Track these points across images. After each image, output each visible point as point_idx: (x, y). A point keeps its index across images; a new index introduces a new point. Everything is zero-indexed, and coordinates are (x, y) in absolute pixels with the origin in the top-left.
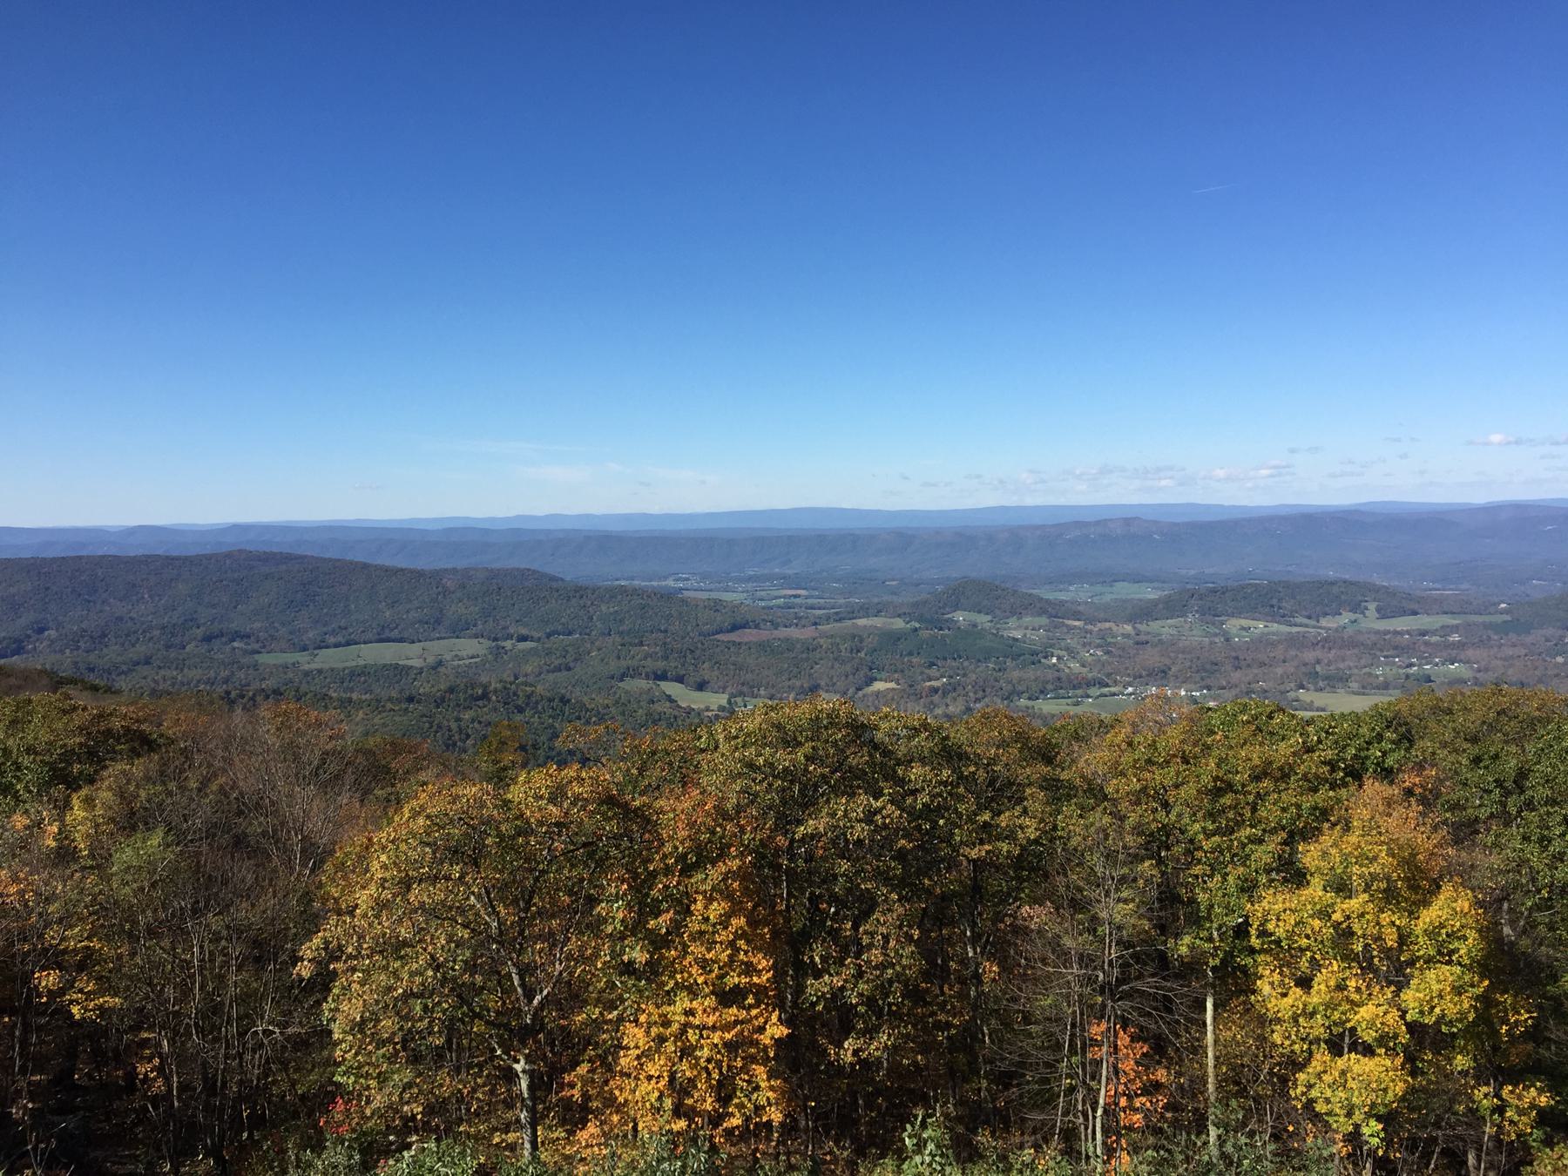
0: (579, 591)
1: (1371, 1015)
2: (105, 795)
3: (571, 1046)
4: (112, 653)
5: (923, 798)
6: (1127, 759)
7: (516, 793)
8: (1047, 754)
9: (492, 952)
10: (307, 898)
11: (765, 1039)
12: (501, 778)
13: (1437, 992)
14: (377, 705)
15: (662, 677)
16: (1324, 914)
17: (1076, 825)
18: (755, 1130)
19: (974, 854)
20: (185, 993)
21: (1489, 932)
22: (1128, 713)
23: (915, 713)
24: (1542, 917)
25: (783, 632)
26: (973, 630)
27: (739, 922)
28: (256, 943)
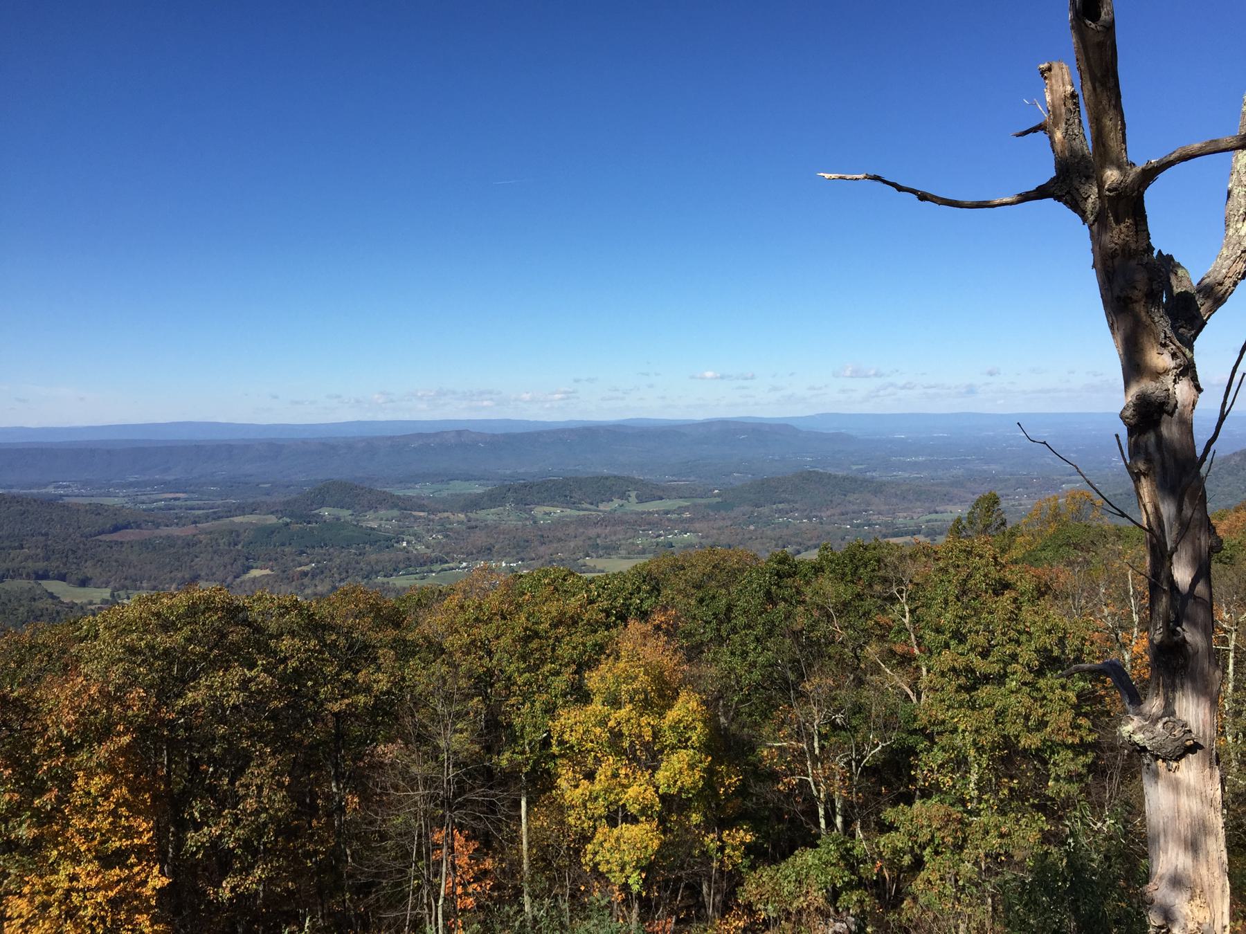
5: (293, 663)
6: (460, 618)
8: (395, 620)
11: (147, 891)
13: (679, 769)
15: (45, 576)
16: (603, 723)
19: (336, 707)
21: (710, 720)
22: (458, 585)
23: (286, 593)
24: (744, 708)
25: (164, 531)
27: (121, 792)
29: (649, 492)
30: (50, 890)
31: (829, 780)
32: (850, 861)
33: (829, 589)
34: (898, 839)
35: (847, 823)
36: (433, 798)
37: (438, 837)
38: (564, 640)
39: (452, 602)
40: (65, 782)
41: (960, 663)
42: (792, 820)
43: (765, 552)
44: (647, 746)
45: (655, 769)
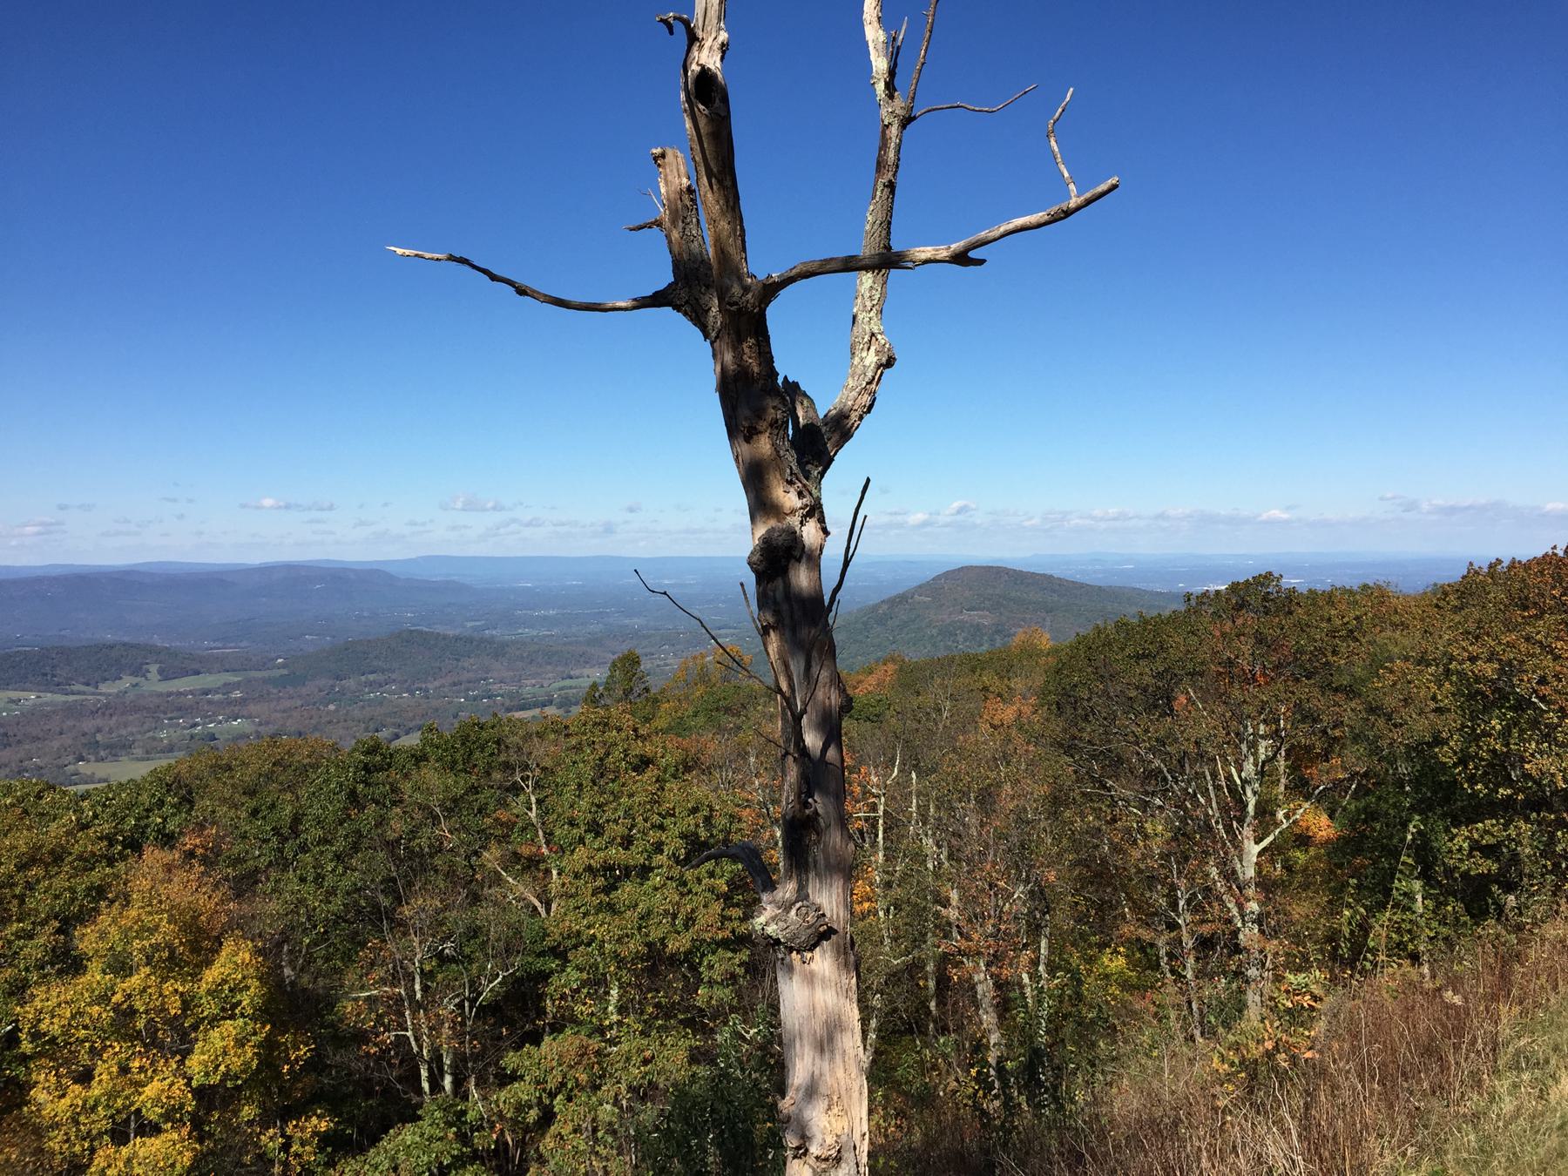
13: (221, 1049)
24: (320, 951)
29: (176, 665)
31: (433, 1032)
33: (435, 781)
34: (523, 1091)
35: (458, 1083)
42: (388, 1091)
43: (349, 739)
44: (173, 1022)
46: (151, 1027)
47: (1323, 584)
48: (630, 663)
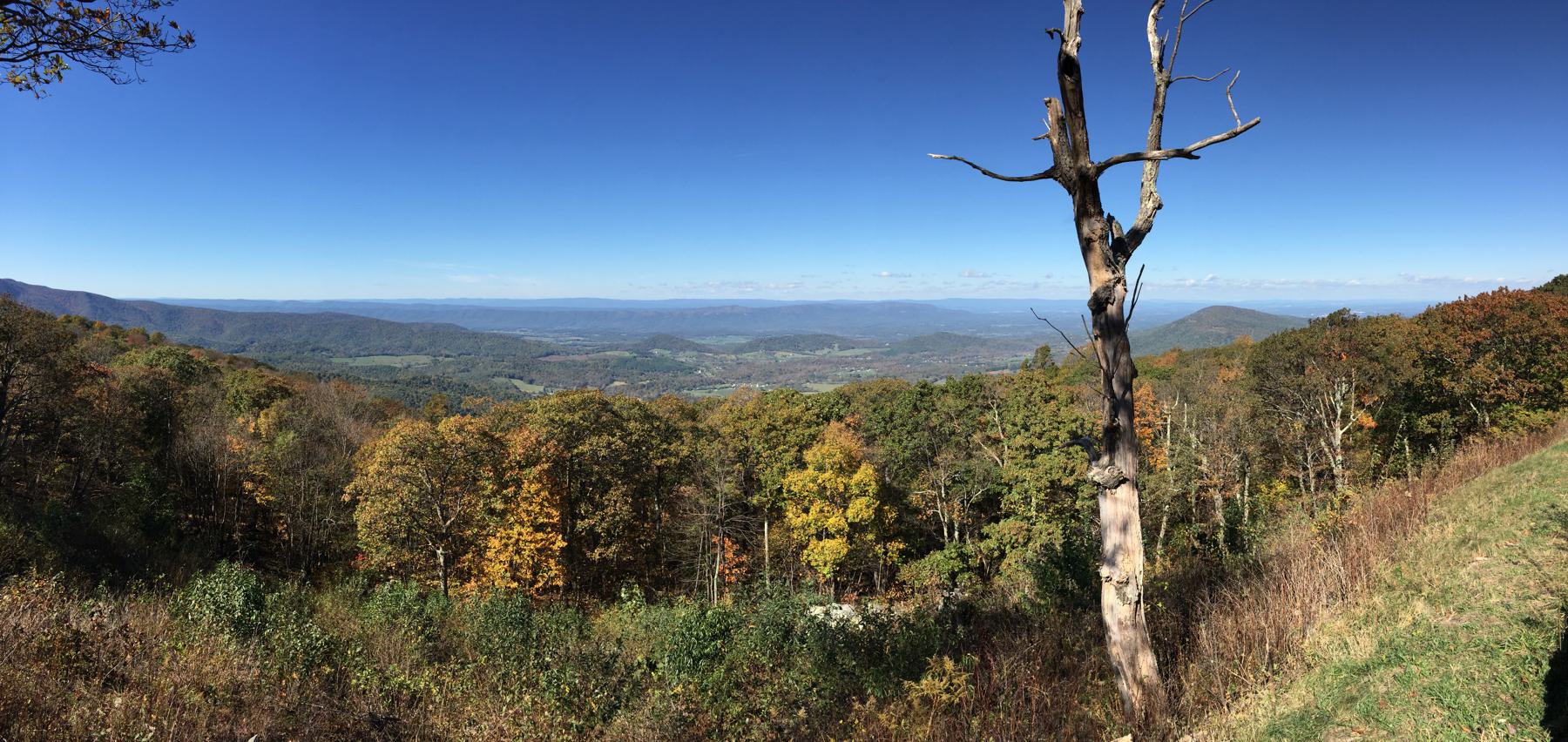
0: (475, 335)
1: (834, 521)
2: (273, 413)
3: (466, 544)
4: (278, 355)
5: (635, 437)
6: (730, 416)
7: (441, 428)
8: (693, 416)
9: (428, 498)
10: (348, 466)
11: (555, 547)
12: (434, 420)
13: (860, 509)
14: (380, 384)
15: (512, 377)
16: (814, 481)
17: (708, 450)
18: (549, 589)
19: (659, 463)
20: (298, 498)
21: (881, 482)
22: (729, 398)
23: (633, 396)
24: (901, 472)
25: (571, 357)
26: (662, 359)
27: (544, 494)
28: (327, 483)
29: (846, 345)
30: (509, 538)
31: (951, 512)
32: (963, 557)
33: (951, 402)
34: (992, 543)
35: (961, 535)
36: (713, 518)
37: (715, 539)
38: (794, 432)
39: (727, 406)
40: (518, 483)
41: (1026, 443)
42: (929, 535)
43: (914, 380)
44: (841, 495)
45: (846, 508)
46: (833, 496)
47: (1374, 314)
48: (1045, 351)
